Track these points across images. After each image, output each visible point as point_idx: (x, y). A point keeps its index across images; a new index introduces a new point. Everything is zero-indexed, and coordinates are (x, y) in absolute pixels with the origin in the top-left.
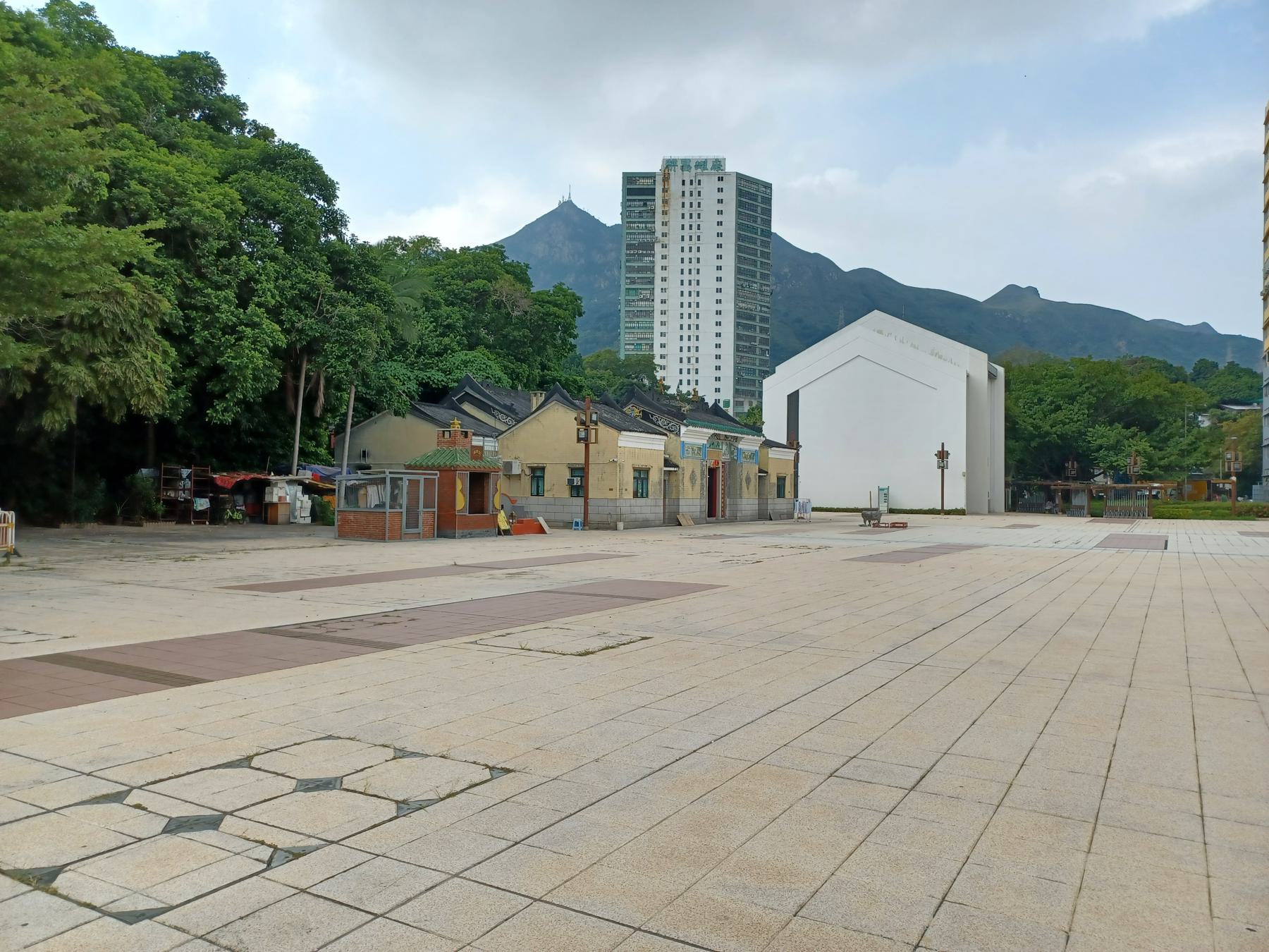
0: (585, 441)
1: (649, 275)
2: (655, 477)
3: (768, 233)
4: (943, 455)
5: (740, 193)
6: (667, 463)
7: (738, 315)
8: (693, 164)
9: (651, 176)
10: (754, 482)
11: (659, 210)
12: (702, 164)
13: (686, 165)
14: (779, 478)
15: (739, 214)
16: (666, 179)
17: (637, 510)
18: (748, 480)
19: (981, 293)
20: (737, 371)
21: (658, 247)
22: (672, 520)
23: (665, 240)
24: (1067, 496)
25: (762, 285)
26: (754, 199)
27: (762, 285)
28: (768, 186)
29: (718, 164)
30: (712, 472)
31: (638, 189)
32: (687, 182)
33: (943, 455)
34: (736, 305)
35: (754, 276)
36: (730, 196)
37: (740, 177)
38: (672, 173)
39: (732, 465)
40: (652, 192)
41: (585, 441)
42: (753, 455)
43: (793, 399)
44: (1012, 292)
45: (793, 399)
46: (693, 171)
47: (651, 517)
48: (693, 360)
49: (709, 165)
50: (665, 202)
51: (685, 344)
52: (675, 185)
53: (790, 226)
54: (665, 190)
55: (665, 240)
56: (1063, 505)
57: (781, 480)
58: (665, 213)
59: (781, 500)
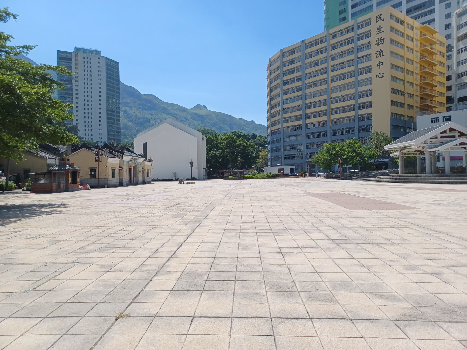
0: (98, 161)
1: (70, 92)
2: (117, 171)
3: (118, 81)
4: (191, 163)
5: (107, 65)
6: (120, 167)
7: (108, 110)
8: (88, 51)
9: (70, 53)
10: (142, 172)
11: (74, 67)
12: (91, 51)
13: (85, 51)
14: (112, 170)
15: (107, 73)
16: (76, 55)
17: (112, 181)
18: (140, 171)
19: (189, 106)
20: (108, 131)
21: (74, 81)
22: (121, 185)
23: (77, 79)
24: (223, 174)
25: (117, 99)
26: (112, 68)
27: (117, 99)
28: (118, 63)
29: (98, 52)
30: (130, 169)
31: (63, 57)
32: (86, 58)
33: (191, 163)
34: (107, 106)
35: (114, 96)
36: (103, 65)
37: (107, 58)
38: (79, 53)
39: (135, 167)
40: (71, 59)
41: (98, 161)
42: (141, 164)
43: (145, 146)
44: (198, 106)
45: (145, 146)
46: (88, 54)
47: (116, 184)
48: (90, 126)
49: (95, 53)
50: (76, 64)
51: (87, 120)
52: (80, 58)
53: (125, 78)
54: (76, 60)
55: (77, 79)
56: (222, 176)
57: (113, 171)
58: (76, 68)
59: (113, 179)
